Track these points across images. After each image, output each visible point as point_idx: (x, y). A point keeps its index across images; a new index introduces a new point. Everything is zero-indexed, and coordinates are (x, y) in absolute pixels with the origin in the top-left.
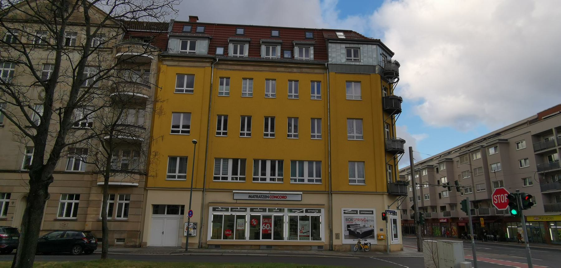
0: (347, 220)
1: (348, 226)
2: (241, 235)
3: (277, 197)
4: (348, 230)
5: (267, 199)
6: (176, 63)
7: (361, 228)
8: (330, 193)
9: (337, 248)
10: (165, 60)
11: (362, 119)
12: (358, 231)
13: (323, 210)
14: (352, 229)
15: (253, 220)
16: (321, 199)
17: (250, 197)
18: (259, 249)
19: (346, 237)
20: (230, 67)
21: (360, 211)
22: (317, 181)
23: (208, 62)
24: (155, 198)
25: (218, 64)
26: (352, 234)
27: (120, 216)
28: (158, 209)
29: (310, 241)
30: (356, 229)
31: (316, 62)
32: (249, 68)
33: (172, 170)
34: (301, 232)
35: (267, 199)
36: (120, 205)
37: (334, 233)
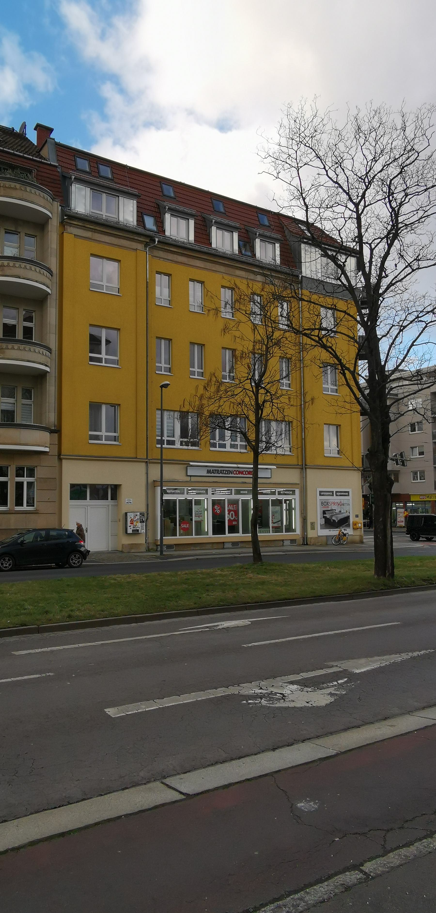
0: (322, 503)
1: (324, 512)
2: (199, 531)
3: (242, 473)
4: (324, 517)
5: (230, 475)
6: (89, 234)
7: (337, 514)
8: (303, 467)
9: (312, 541)
10: (71, 225)
11: (119, 329)
12: (334, 518)
13: (297, 491)
14: (328, 516)
15: (216, 507)
16: (292, 476)
17: (209, 472)
18: (224, 548)
19: (322, 527)
20: (170, 256)
21: (336, 492)
22: (108, 438)
23: (141, 242)
24: (74, 473)
25: (155, 248)
26: (329, 523)
27: (22, 505)
28: (78, 492)
29: (271, 534)
30: (332, 516)
31: (197, 248)
32: (198, 263)
33: (95, 425)
34: (273, 523)
35: (230, 475)
36: (19, 486)
37: (309, 521)
